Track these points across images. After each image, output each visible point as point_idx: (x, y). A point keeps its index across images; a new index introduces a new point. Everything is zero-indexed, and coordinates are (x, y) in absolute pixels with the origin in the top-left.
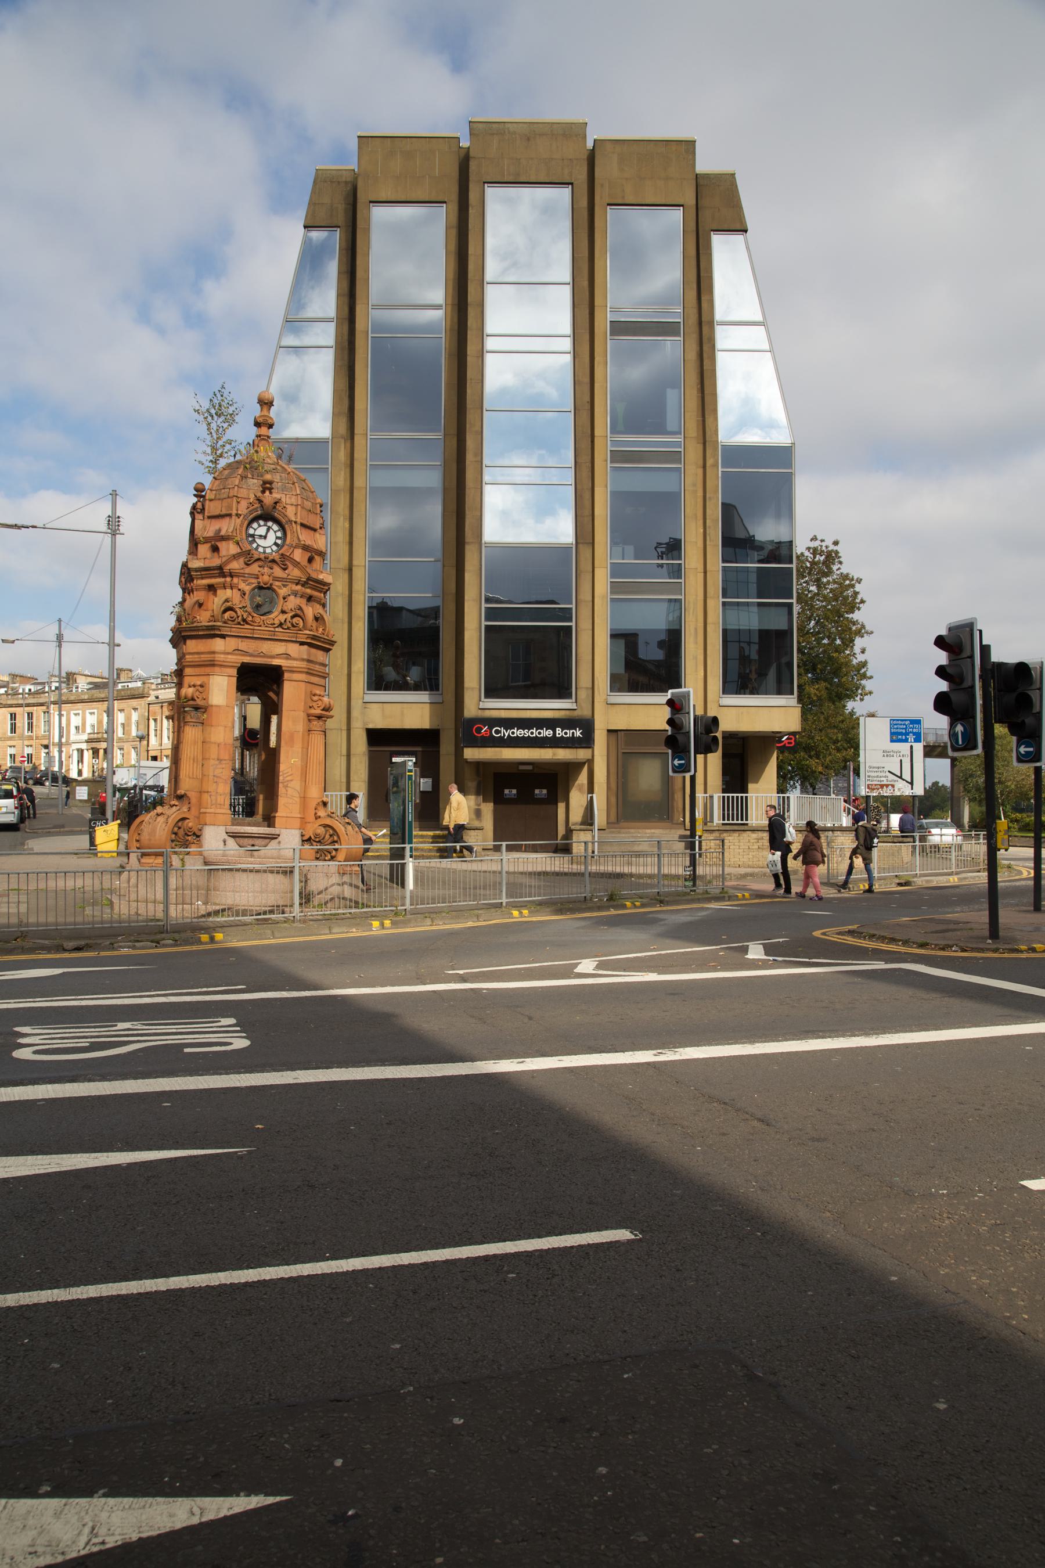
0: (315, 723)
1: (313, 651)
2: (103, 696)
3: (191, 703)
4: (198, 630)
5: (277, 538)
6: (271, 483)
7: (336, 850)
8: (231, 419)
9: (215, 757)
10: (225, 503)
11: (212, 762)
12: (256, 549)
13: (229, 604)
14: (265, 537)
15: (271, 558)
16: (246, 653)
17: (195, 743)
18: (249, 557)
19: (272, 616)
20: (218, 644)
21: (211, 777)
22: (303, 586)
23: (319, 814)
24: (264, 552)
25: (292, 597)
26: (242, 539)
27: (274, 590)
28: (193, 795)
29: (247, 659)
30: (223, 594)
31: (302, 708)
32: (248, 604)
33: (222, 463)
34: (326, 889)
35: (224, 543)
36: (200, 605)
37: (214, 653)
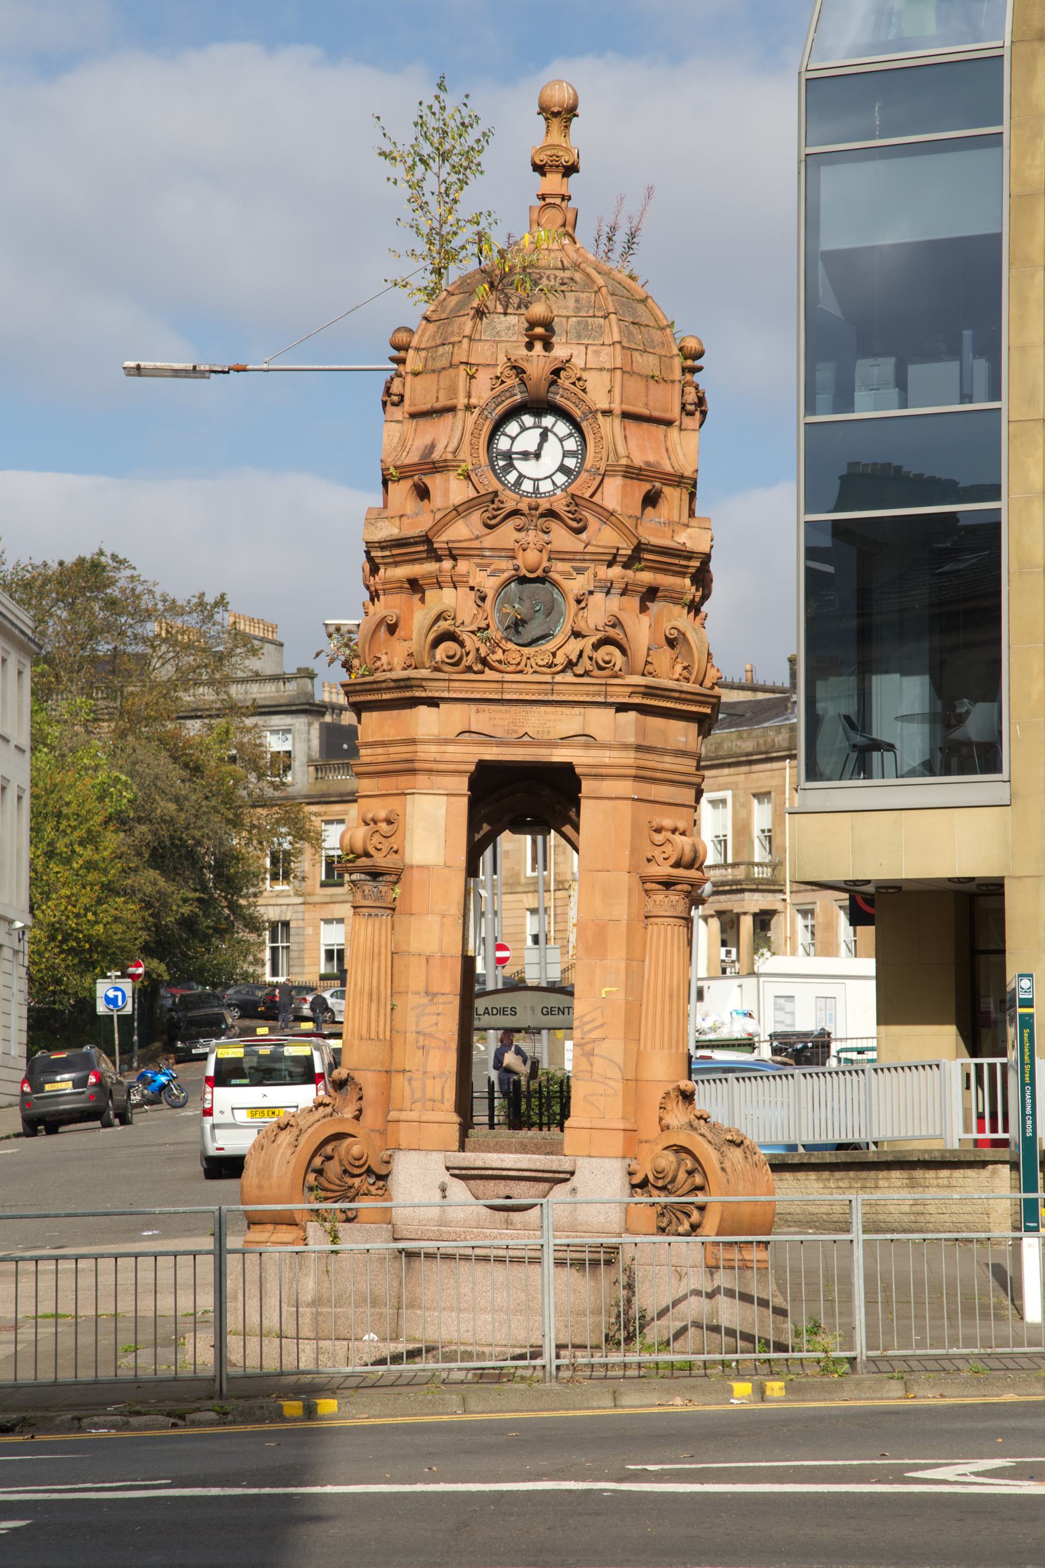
0: (659, 897)
1: (655, 723)
2: (748, 746)
3: (363, 861)
4: (379, 690)
5: (566, 454)
6: (548, 325)
7: (702, 1208)
8: (466, 166)
9: (421, 987)
10: (445, 378)
11: (413, 1000)
12: (518, 482)
13: (443, 625)
14: (537, 456)
15: (544, 504)
16: (489, 739)
17: (373, 955)
18: (492, 509)
19: (550, 646)
20: (425, 721)
21: (411, 1037)
22: (626, 566)
23: (671, 1120)
24: (536, 489)
25: (599, 597)
26: (477, 467)
27: (554, 584)
28: (369, 1081)
29: (492, 753)
30: (447, 598)
31: (626, 865)
32: (494, 621)
33: (454, 273)
34: (675, 1304)
35: (438, 476)
36: (392, 629)
37: (413, 742)
